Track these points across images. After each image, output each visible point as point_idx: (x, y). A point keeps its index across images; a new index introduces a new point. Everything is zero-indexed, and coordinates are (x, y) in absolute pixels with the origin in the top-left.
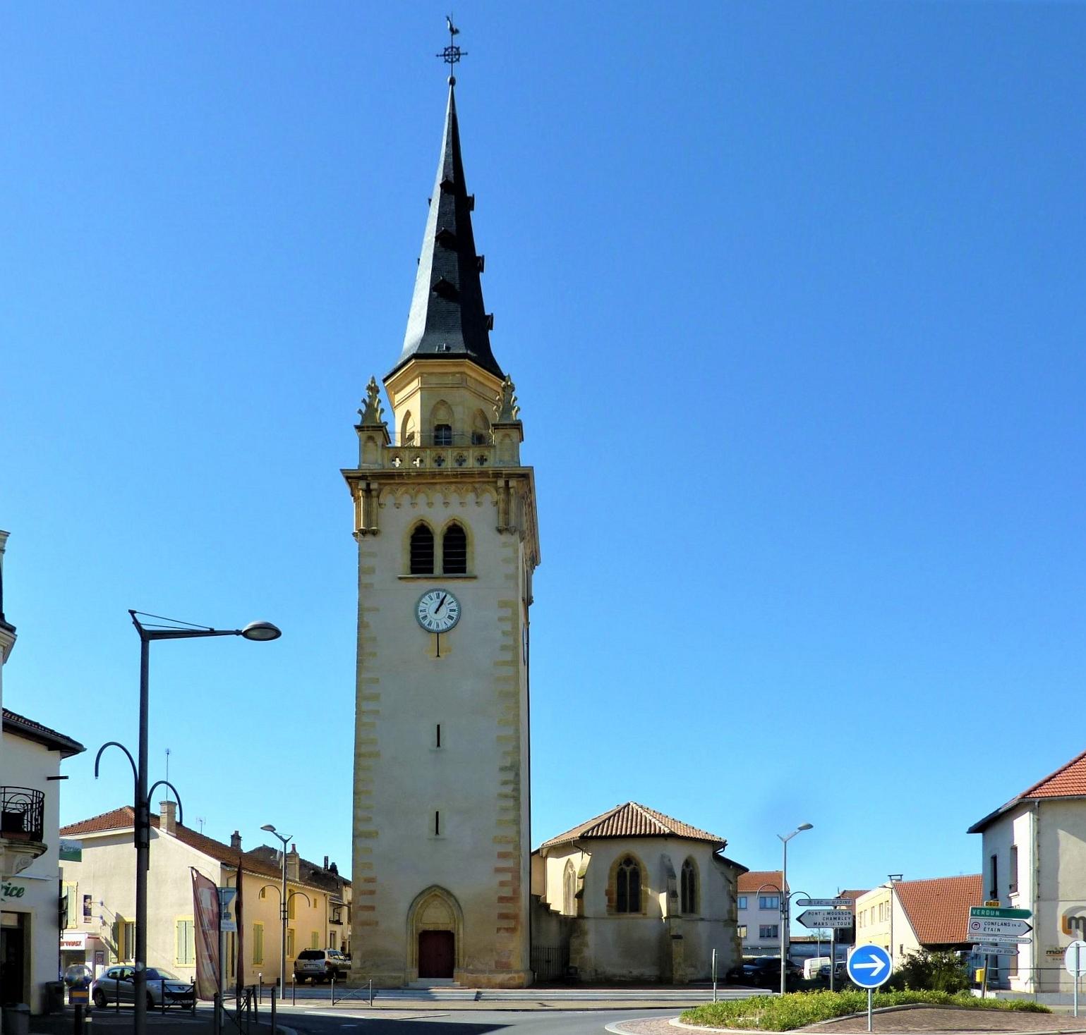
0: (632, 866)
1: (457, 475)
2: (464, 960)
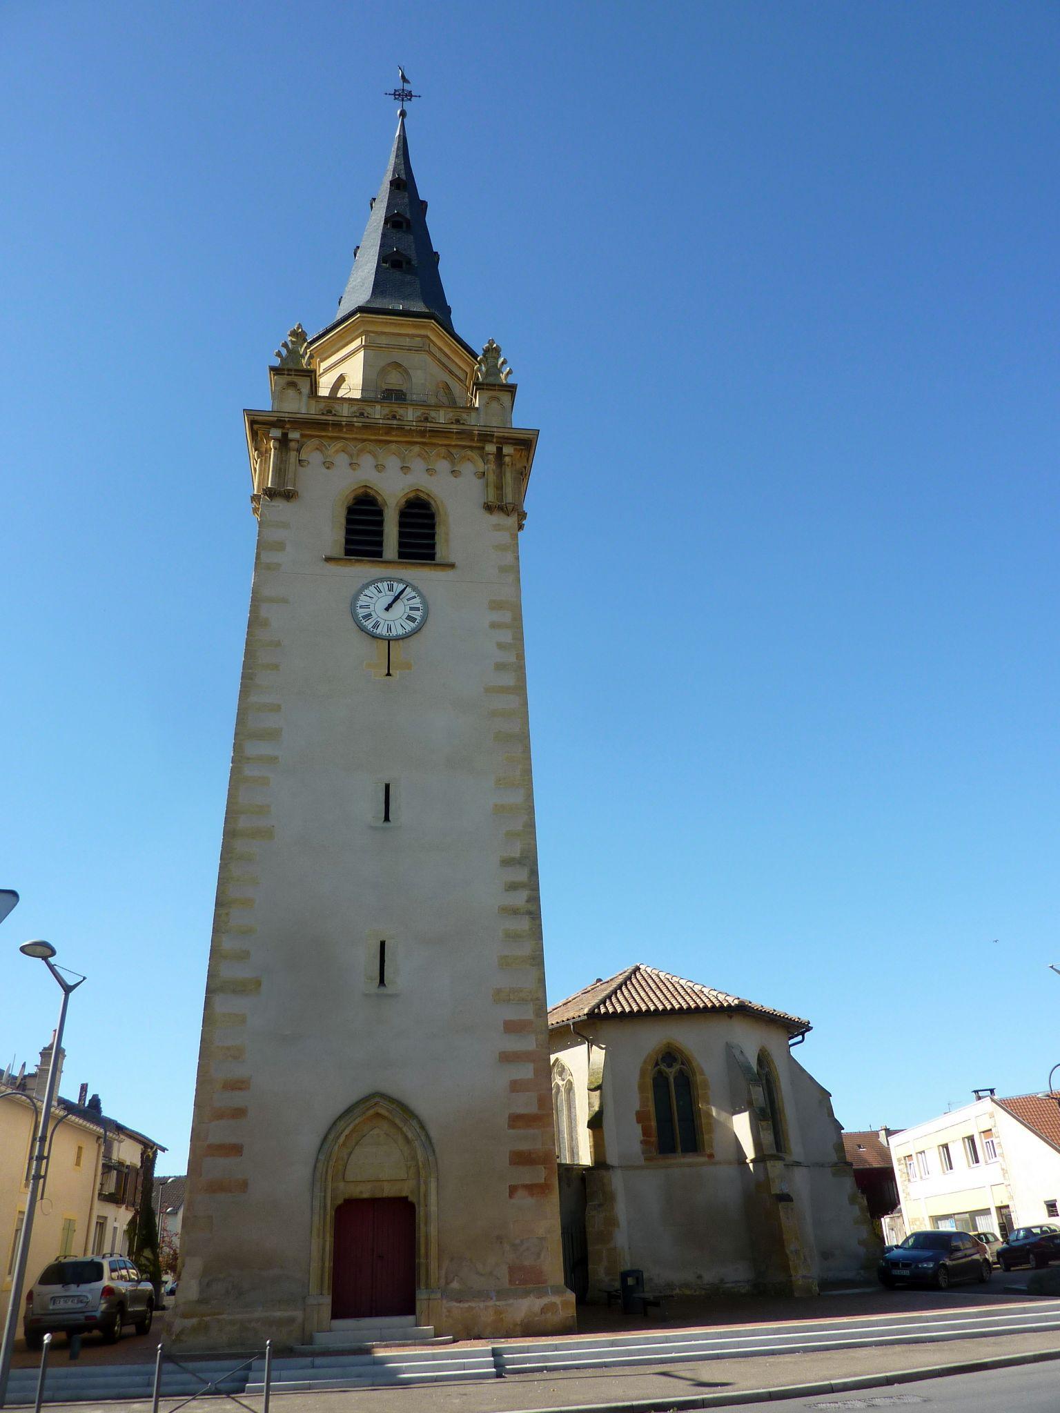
0: (676, 1067)
1: (425, 431)
2: (439, 1267)
